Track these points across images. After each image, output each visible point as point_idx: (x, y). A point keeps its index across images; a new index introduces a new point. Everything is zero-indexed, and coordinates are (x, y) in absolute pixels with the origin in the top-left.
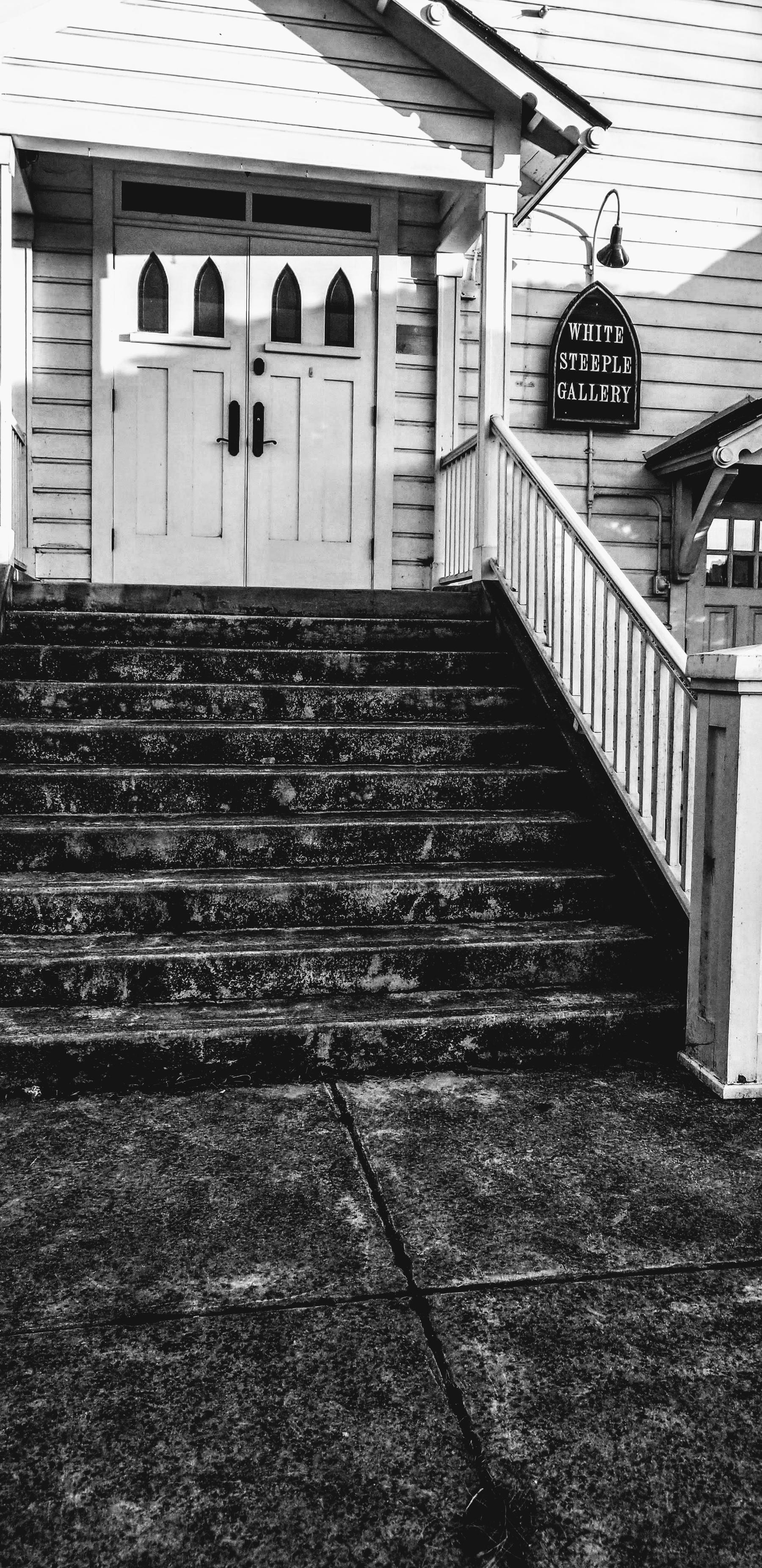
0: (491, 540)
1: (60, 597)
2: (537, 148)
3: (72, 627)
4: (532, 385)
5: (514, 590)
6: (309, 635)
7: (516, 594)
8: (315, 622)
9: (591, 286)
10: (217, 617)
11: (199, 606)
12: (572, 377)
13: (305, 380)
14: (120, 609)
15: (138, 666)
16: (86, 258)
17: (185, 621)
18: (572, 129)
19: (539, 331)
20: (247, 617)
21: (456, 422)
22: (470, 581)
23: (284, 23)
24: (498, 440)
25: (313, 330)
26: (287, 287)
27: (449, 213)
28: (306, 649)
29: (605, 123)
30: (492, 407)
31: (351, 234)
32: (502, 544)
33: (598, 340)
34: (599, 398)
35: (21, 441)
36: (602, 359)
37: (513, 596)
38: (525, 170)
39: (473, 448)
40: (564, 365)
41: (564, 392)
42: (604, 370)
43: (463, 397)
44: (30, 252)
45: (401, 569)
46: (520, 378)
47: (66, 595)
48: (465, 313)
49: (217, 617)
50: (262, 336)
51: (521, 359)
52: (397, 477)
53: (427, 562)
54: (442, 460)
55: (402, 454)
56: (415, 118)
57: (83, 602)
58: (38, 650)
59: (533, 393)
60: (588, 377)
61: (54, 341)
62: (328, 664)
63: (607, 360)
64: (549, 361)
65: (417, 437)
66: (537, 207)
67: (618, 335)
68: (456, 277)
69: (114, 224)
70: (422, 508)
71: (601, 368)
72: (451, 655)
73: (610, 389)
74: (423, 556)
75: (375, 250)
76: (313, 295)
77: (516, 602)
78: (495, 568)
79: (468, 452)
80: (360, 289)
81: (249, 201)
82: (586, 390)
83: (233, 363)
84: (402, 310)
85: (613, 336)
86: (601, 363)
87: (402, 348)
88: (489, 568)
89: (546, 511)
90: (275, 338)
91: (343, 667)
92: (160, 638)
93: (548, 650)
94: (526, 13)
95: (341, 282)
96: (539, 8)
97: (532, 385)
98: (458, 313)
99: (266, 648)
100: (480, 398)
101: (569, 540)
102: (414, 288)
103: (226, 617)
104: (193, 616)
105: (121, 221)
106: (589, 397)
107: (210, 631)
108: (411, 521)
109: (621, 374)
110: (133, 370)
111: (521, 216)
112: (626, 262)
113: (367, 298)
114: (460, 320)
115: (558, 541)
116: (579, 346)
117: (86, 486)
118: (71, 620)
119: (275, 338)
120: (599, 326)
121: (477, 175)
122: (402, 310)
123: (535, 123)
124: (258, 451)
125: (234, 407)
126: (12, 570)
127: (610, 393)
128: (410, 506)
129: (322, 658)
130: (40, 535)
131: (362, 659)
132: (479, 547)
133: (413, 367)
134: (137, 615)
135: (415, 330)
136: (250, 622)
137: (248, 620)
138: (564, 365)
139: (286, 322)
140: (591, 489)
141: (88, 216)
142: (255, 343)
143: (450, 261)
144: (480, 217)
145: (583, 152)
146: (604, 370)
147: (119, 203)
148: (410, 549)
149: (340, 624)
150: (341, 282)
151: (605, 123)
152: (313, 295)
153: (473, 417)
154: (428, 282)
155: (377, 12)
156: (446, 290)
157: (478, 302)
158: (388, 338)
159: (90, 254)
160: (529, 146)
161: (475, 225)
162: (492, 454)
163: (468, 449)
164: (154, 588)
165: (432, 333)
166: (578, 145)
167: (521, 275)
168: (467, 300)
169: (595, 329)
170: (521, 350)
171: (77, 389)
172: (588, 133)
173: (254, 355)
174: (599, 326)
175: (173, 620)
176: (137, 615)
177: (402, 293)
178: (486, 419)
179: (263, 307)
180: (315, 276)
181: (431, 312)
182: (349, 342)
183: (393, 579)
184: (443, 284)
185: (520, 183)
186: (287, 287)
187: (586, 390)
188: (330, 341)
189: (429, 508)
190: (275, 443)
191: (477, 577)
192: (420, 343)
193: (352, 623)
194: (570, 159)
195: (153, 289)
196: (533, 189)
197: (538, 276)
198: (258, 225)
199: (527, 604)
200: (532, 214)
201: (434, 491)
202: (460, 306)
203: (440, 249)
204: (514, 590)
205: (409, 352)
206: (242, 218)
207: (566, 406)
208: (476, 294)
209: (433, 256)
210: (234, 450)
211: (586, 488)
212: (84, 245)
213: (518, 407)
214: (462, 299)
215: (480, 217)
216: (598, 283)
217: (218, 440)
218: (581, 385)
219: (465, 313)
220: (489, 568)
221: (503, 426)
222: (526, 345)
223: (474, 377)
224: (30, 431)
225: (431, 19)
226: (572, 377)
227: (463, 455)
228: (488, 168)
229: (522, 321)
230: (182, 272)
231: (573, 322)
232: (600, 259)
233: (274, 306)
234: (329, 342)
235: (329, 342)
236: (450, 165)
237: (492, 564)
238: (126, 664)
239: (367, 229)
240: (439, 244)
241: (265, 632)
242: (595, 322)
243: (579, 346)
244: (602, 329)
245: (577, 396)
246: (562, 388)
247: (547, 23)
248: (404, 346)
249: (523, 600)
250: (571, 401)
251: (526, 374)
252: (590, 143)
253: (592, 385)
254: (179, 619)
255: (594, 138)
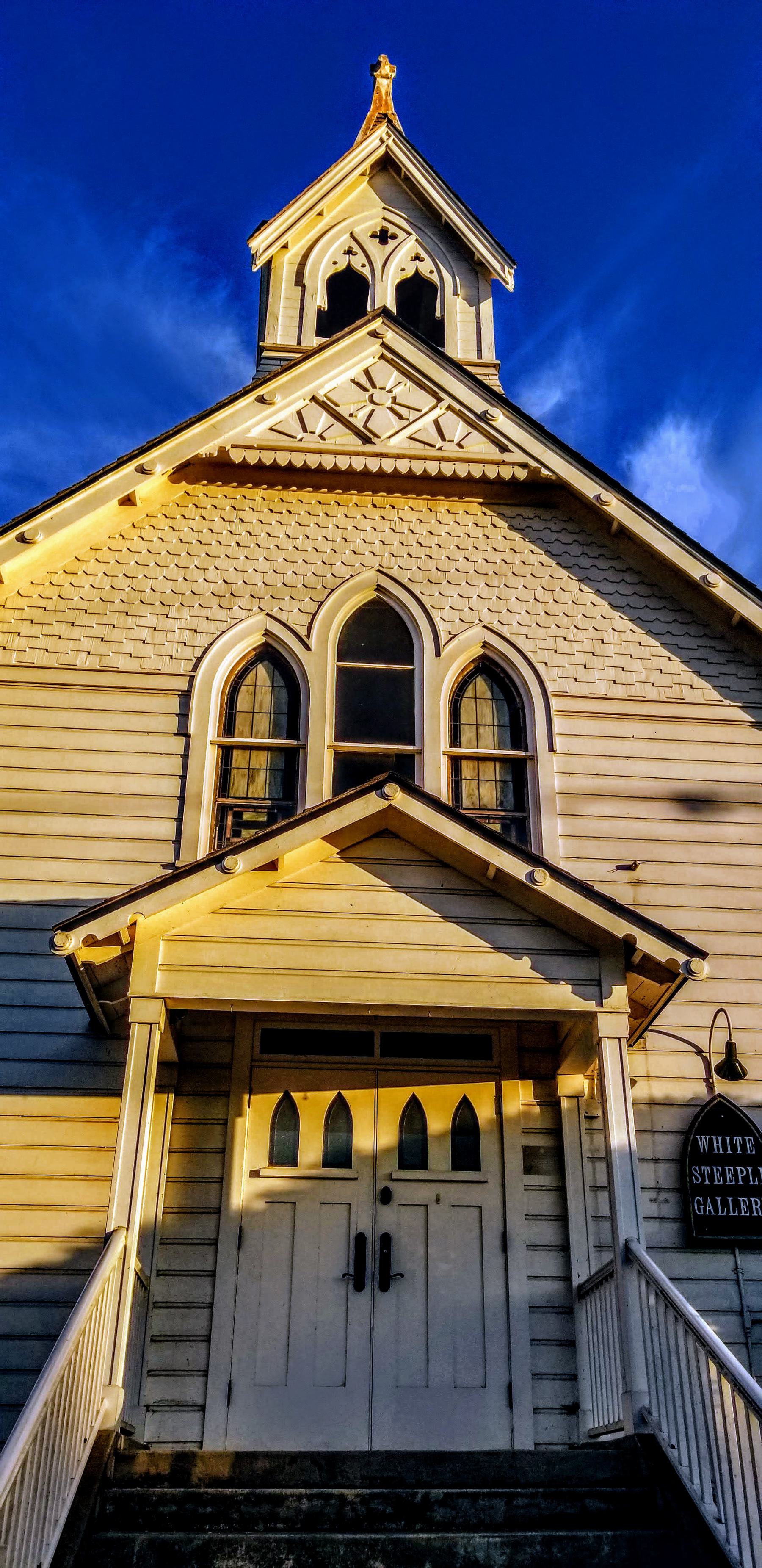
0: (641, 1384)
1: (164, 1468)
2: (643, 979)
3: (174, 1508)
4: (666, 1201)
5: (673, 1447)
6: (439, 1514)
7: (675, 1452)
8: (446, 1495)
9: (714, 1099)
10: (336, 1491)
11: (317, 1477)
12: (709, 1191)
13: (433, 1208)
14: (228, 1483)
15: (243, 1560)
16: (224, 1099)
17: (300, 1497)
18: (673, 961)
19: (667, 1145)
20: (368, 1491)
21: (591, 1244)
22: (621, 1435)
23: (406, 893)
24: (636, 1266)
25: (439, 1157)
26: (413, 1115)
27: (566, 1037)
28: (437, 1531)
29: (703, 955)
30: (626, 1230)
31: (475, 1063)
32: (653, 1387)
33: (729, 1152)
34: (740, 1212)
35: (143, 1285)
36: (736, 1171)
37: (673, 1454)
38: (634, 997)
39: (611, 1275)
40: (697, 1179)
41: (703, 1208)
42: (741, 1183)
43: (596, 1217)
44: (172, 1096)
45: (546, 1420)
46: (653, 1194)
47: (172, 1466)
48: (591, 1131)
49: (336, 1491)
50: (390, 1165)
51: (652, 1176)
52: (533, 1308)
53: (572, 1409)
54: (580, 1287)
55: (536, 1283)
56: (526, 961)
57: (189, 1474)
58: (133, 1540)
59: (669, 1210)
60: (725, 1191)
61: (183, 1151)
62: (462, 1552)
63: (742, 1171)
64: (683, 1175)
65: (549, 1264)
66: (650, 1028)
67: (749, 1146)
68: (577, 1097)
69: (252, 1067)
70: (561, 1343)
71: (737, 1181)
72: (607, 1537)
73: (750, 1202)
74: (568, 1402)
75: (497, 1075)
76: (438, 1122)
77: (677, 1464)
78: (648, 1419)
79: (606, 1279)
80: (485, 1112)
81: (377, 1051)
82: (725, 1204)
83: (360, 1193)
84: (526, 1132)
85: (744, 1147)
86: (735, 1175)
87: (528, 1170)
88: (642, 1418)
89: (696, 1351)
90: (402, 1165)
91: (481, 1555)
92: (270, 1521)
93: (721, 1528)
94: (619, 868)
95: (465, 1104)
96: (631, 863)
97: (666, 1201)
98: (583, 1132)
99: (391, 1531)
100: (612, 1218)
101: (727, 1387)
102: (537, 1109)
103: (346, 1491)
104: (309, 1491)
105: (257, 1064)
106: (728, 1212)
107: (328, 1509)
108: (550, 1360)
109: (739, 1216)
110: (260, 1205)
111: (636, 1036)
112: (745, 1075)
113: (490, 1121)
114: (585, 1138)
115: (715, 1387)
116: (711, 1158)
117: (203, 1368)
118: (174, 1499)
119: (402, 1165)
120: (728, 1138)
121: (590, 1006)
122: (526, 1132)
123: (637, 958)
124: (384, 1287)
125: (361, 1239)
126: (118, 1436)
127: (750, 1206)
128: (547, 1342)
129: (456, 1544)
130: (154, 1390)
131: (503, 1544)
132: (628, 1392)
133: (541, 1188)
134: (246, 1491)
135: (542, 1151)
136: (373, 1496)
137: (370, 1494)
138: (697, 1179)
139: (412, 1150)
140: (747, 1315)
141: (227, 1060)
142: (383, 1171)
143: (572, 1083)
144: (595, 1043)
145: (685, 980)
146: (741, 1183)
147: (257, 1048)
148: (552, 1393)
149: (475, 1497)
150: (465, 1104)
151: (703, 955)
152: (438, 1122)
153: (607, 1238)
154: (549, 1100)
155: (488, 879)
156: (569, 1110)
157: (601, 1119)
158: (515, 1161)
159: (227, 1095)
160: (633, 976)
161: (589, 1050)
162: (633, 1285)
163: (603, 1278)
164: (267, 1455)
165: (558, 1153)
166: (679, 974)
167: (641, 1091)
168: (591, 1118)
169: (724, 1141)
170: (652, 1165)
171: (204, 1227)
172: (688, 963)
173: (382, 1184)
174: (728, 1138)
175: (286, 1497)
176: (246, 1491)
177: (526, 1115)
178: (622, 1241)
179: (388, 1136)
180: (439, 1105)
181: (556, 1132)
182: (476, 1166)
183: (536, 1433)
184: (565, 1104)
185: (629, 1010)
186: (413, 1115)
187: (725, 1204)
188: (457, 1166)
189: (569, 1344)
190: (402, 1276)
191: (629, 1429)
192: (546, 1164)
193: (490, 1496)
194: (674, 986)
195: (286, 1117)
196: (642, 1016)
197: (659, 1090)
198: (387, 1060)
199: (690, 1466)
200: (648, 1034)
201: (573, 1323)
202: (584, 1125)
203: (559, 1072)
204: (673, 1447)
205: (538, 1172)
206: (371, 1054)
207: (705, 1222)
208: (599, 1113)
209: (554, 1078)
210: (359, 1287)
211: (741, 1313)
212: (224, 1088)
213: (653, 1226)
214: (586, 1117)
215: (595, 1043)
216: (720, 1095)
217: (344, 1276)
218: (719, 1199)
219: (591, 1131)
220: (642, 1418)
221: (641, 1250)
222: (656, 1160)
223: (604, 1196)
224: (154, 1273)
225: (534, 881)
226: (709, 1191)
227: (601, 1283)
228: (598, 999)
229: (648, 1136)
230: (313, 1106)
231: (700, 1135)
232: (718, 1073)
233: (401, 1132)
234: (456, 1167)
235: (456, 1167)
236: (561, 997)
237: (645, 1413)
238: (230, 1557)
239: (489, 1057)
240: (559, 1067)
241: (389, 1510)
242: (723, 1134)
243: (711, 1158)
244: (731, 1140)
245: (716, 1211)
246: (699, 1202)
247: (642, 872)
248: (531, 1167)
249: (685, 1461)
250: (710, 1216)
251: (659, 1190)
252: (691, 973)
253: (730, 1199)
254: (292, 1495)
255: (693, 967)
